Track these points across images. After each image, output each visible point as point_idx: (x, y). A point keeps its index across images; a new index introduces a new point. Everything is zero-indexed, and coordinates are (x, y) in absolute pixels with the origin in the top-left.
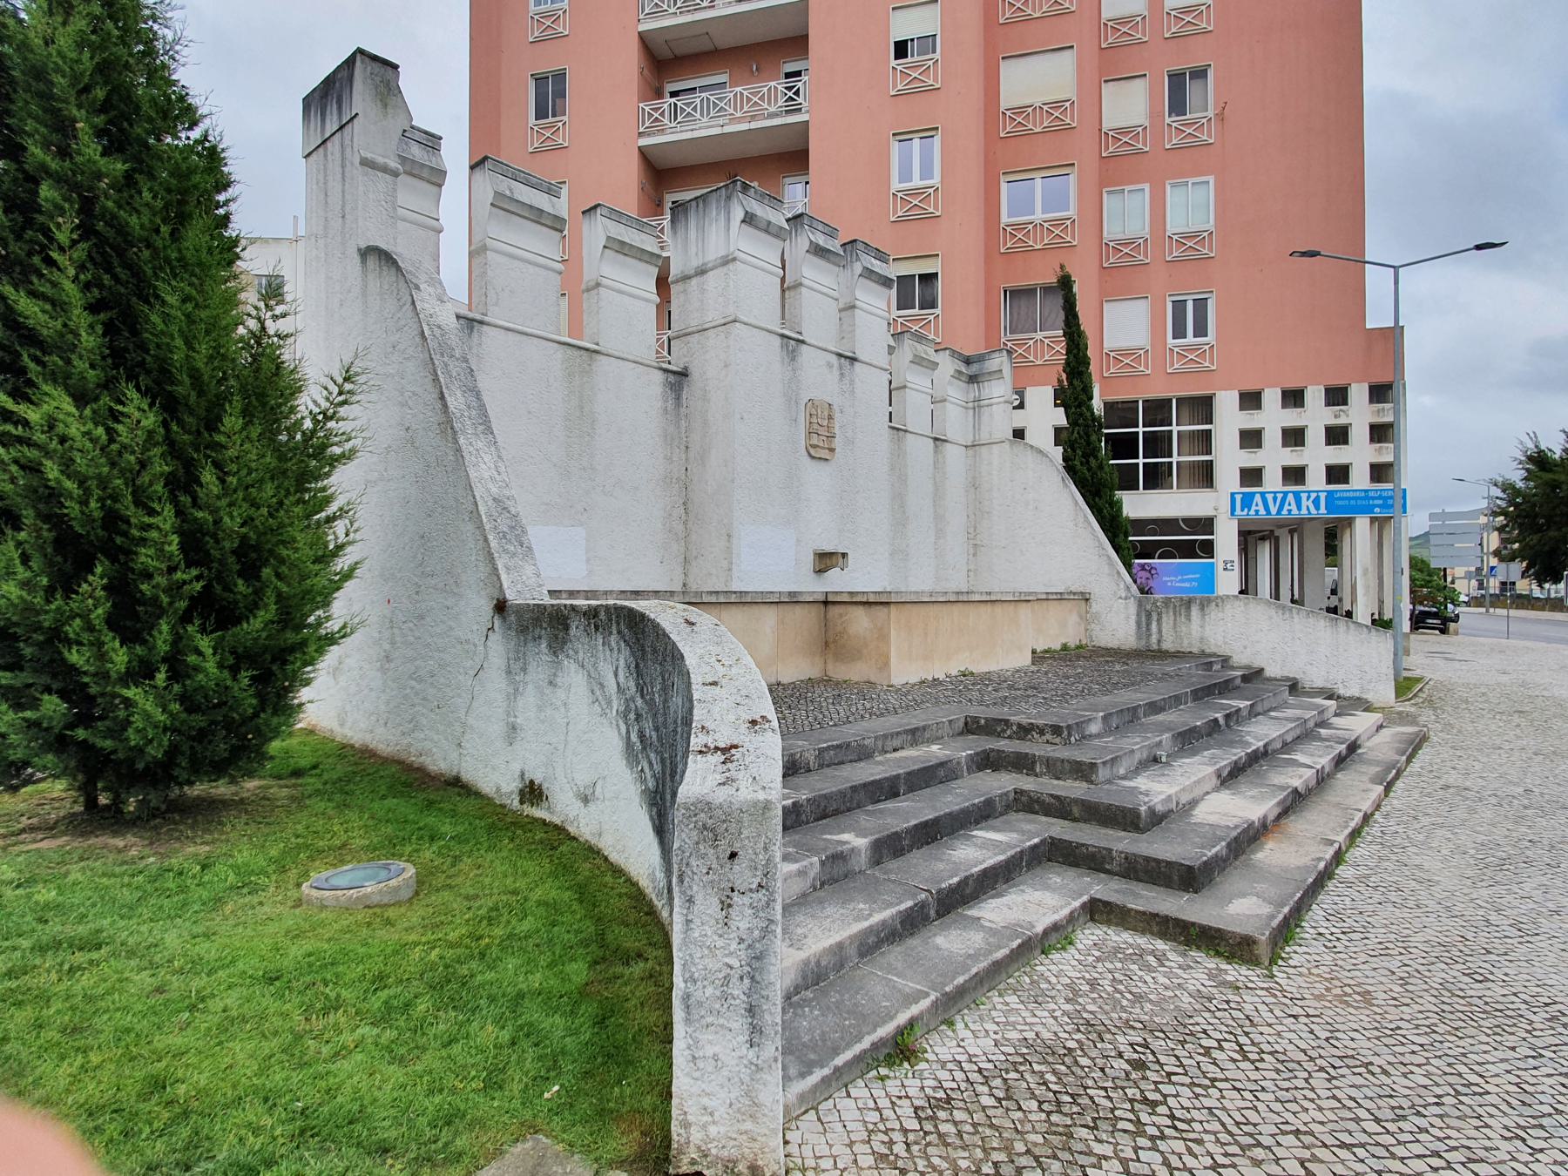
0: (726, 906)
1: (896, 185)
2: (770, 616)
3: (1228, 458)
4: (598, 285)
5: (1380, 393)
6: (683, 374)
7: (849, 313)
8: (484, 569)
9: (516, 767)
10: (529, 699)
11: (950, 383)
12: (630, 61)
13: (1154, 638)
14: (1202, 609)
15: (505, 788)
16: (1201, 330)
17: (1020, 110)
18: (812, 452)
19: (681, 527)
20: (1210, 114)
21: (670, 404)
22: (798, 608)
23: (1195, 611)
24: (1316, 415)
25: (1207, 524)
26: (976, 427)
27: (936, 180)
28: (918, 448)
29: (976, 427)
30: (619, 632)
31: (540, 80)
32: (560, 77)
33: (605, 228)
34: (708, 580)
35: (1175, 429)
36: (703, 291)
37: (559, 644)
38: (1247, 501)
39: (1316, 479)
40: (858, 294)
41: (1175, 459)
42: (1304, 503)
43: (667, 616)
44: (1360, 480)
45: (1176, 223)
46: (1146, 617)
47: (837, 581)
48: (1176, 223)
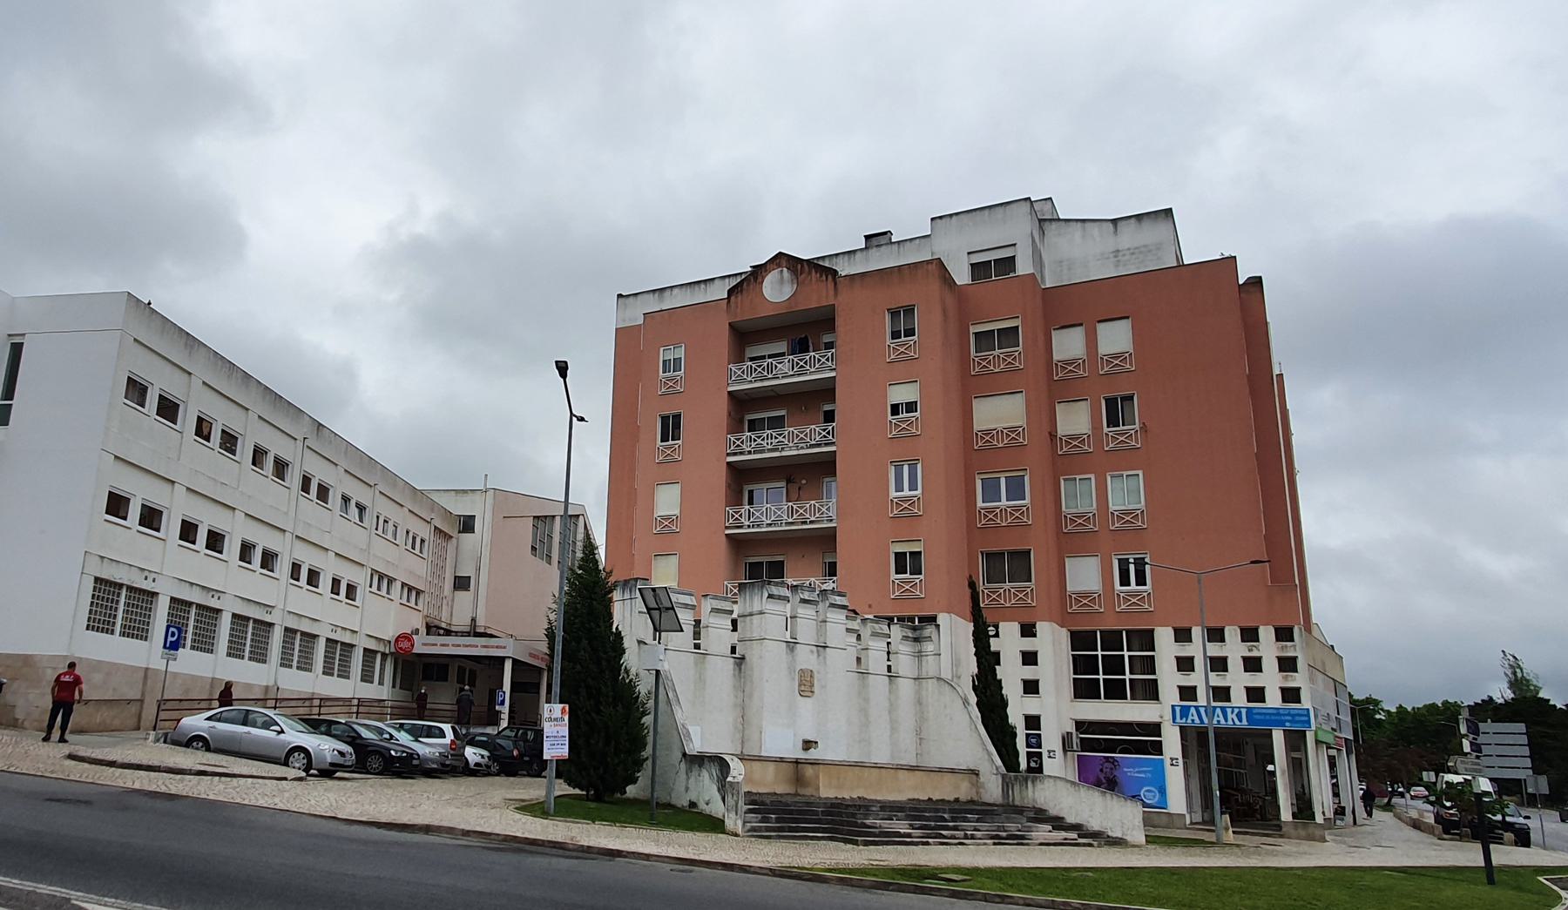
1: (893, 494)
2: (771, 767)
3: (1169, 679)
5: (1284, 634)
6: (743, 658)
10: (692, 780)
12: (722, 406)
16: (1141, 580)
17: (987, 432)
20: (1137, 426)
24: (1234, 648)
25: (1155, 729)
26: (920, 667)
27: (918, 492)
28: (879, 683)
29: (920, 667)
31: (665, 419)
32: (677, 417)
35: (1126, 654)
38: (1185, 711)
39: (1239, 699)
41: (1128, 676)
42: (1230, 716)
43: (727, 758)
44: (1273, 700)
45: (1114, 505)
46: (1006, 785)
47: (813, 754)
48: (1114, 505)
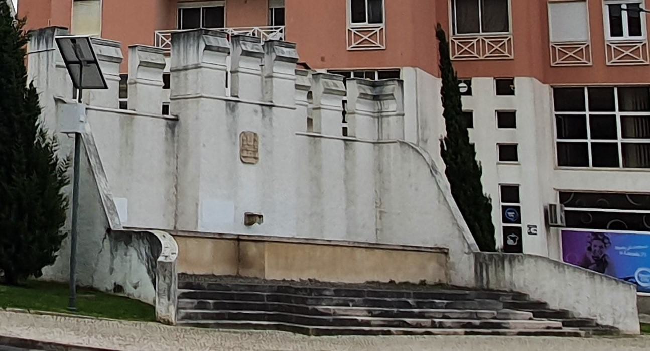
0: (164, 278)
2: (209, 244)
4: (135, 83)
6: (176, 119)
7: (269, 79)
8: (103, 218)
9: (113, 282)
10: (118, 260)
11: (358, 102)
13: (485, 281)
14: (510, 262)
15: (109, 288)
16: (635, 30)
18: (244, 159)
19: (174, 198)
21: (170, 134)
22: (223, 241)
23: (507, 264)
28: (333, 149)
30: (147, 239)
33: (140, 57)
34: (186, 225)
35: (618, 114)
36: (186, 79)
37: (128, 243)
40: (275, 70)
41: (620, 140)
43: (158, 234)
46: (480, 265)
47: (257, 230)
